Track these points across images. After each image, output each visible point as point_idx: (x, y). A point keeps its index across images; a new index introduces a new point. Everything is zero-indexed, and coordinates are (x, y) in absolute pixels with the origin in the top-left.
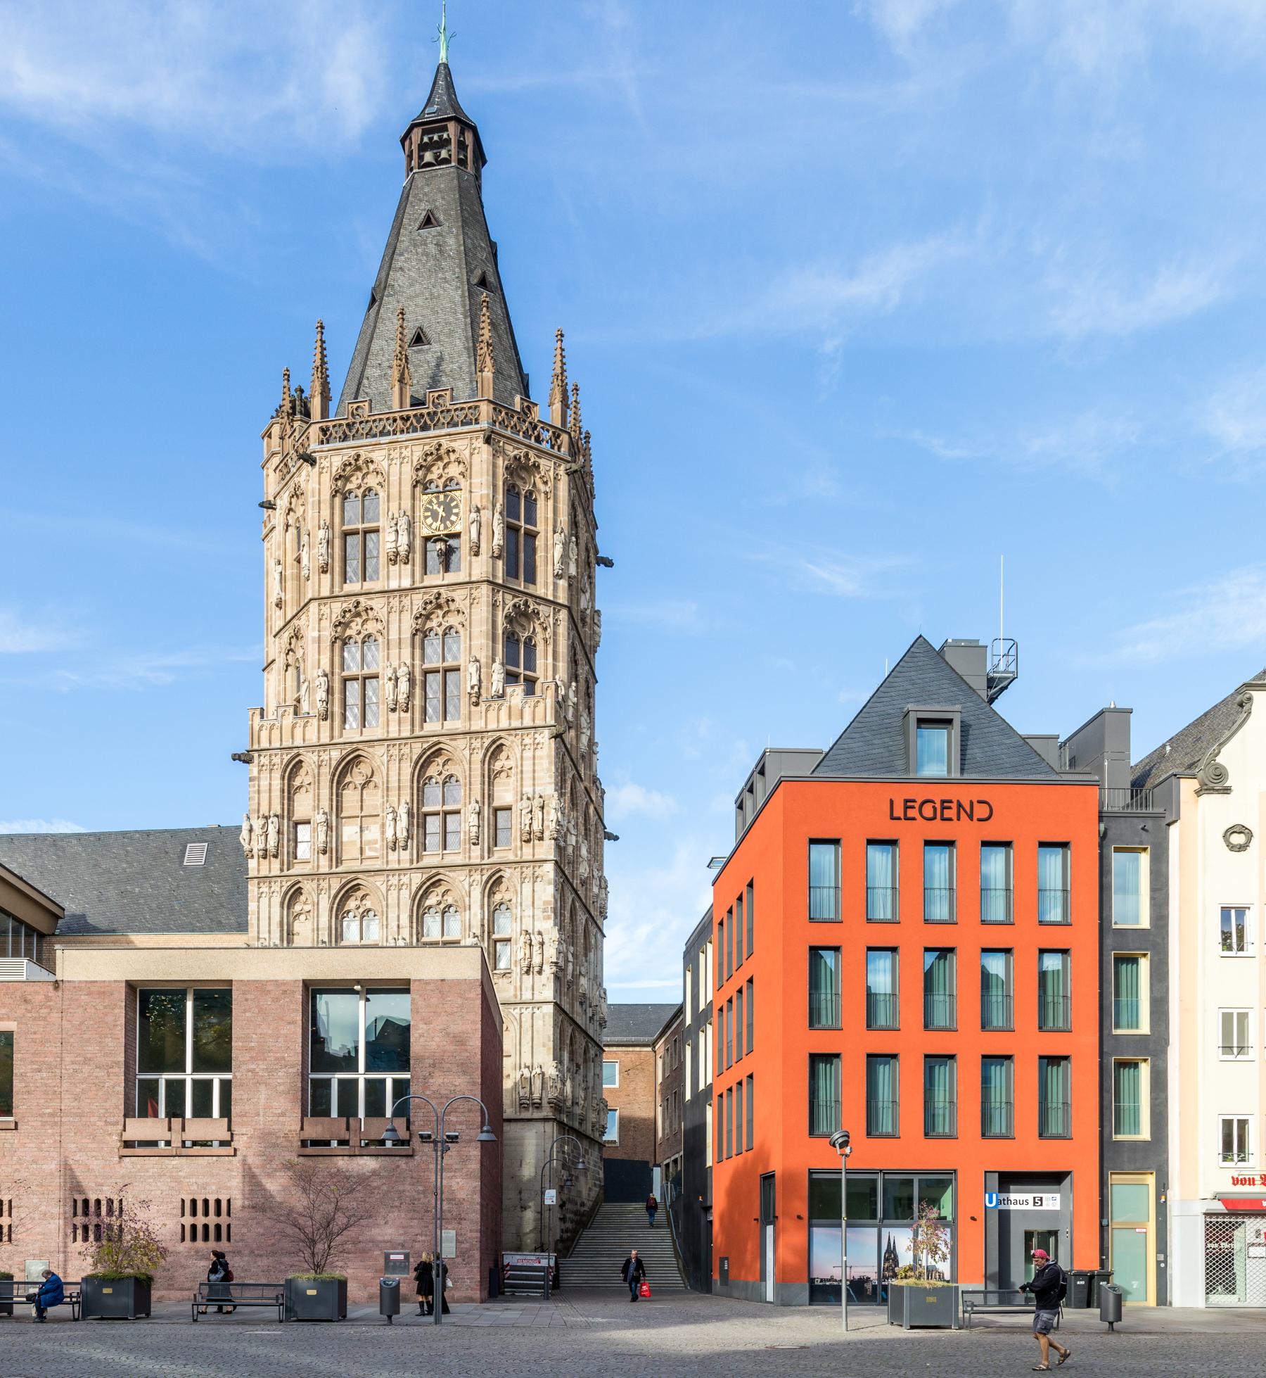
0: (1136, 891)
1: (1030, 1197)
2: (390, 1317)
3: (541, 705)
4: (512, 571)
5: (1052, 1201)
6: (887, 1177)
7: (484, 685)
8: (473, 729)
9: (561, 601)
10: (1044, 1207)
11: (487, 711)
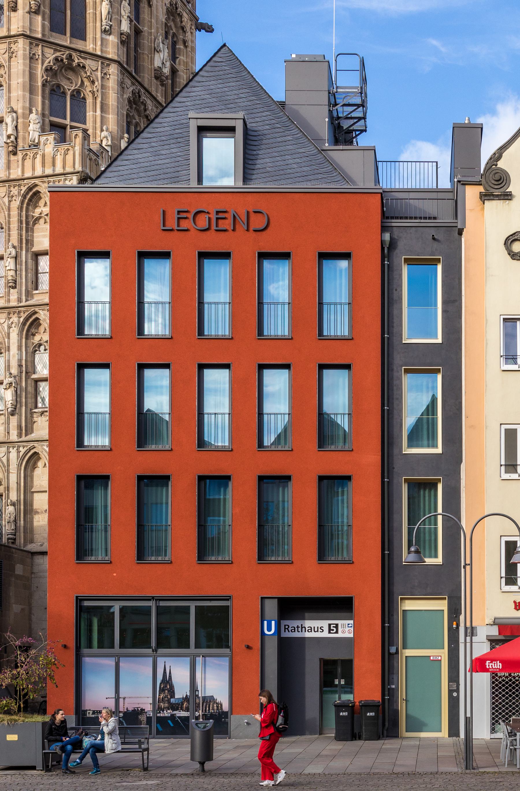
0: (436, 305)
1: (325, 624)
2: (202, 764)
3: (71, 152)
4: (56, 25)
5: (345, 629)
6: (162, 604)
7: (21, 134)
8: (12, 177)
9: (110, 56)
10: (340, 635)
11: (24, 159)
